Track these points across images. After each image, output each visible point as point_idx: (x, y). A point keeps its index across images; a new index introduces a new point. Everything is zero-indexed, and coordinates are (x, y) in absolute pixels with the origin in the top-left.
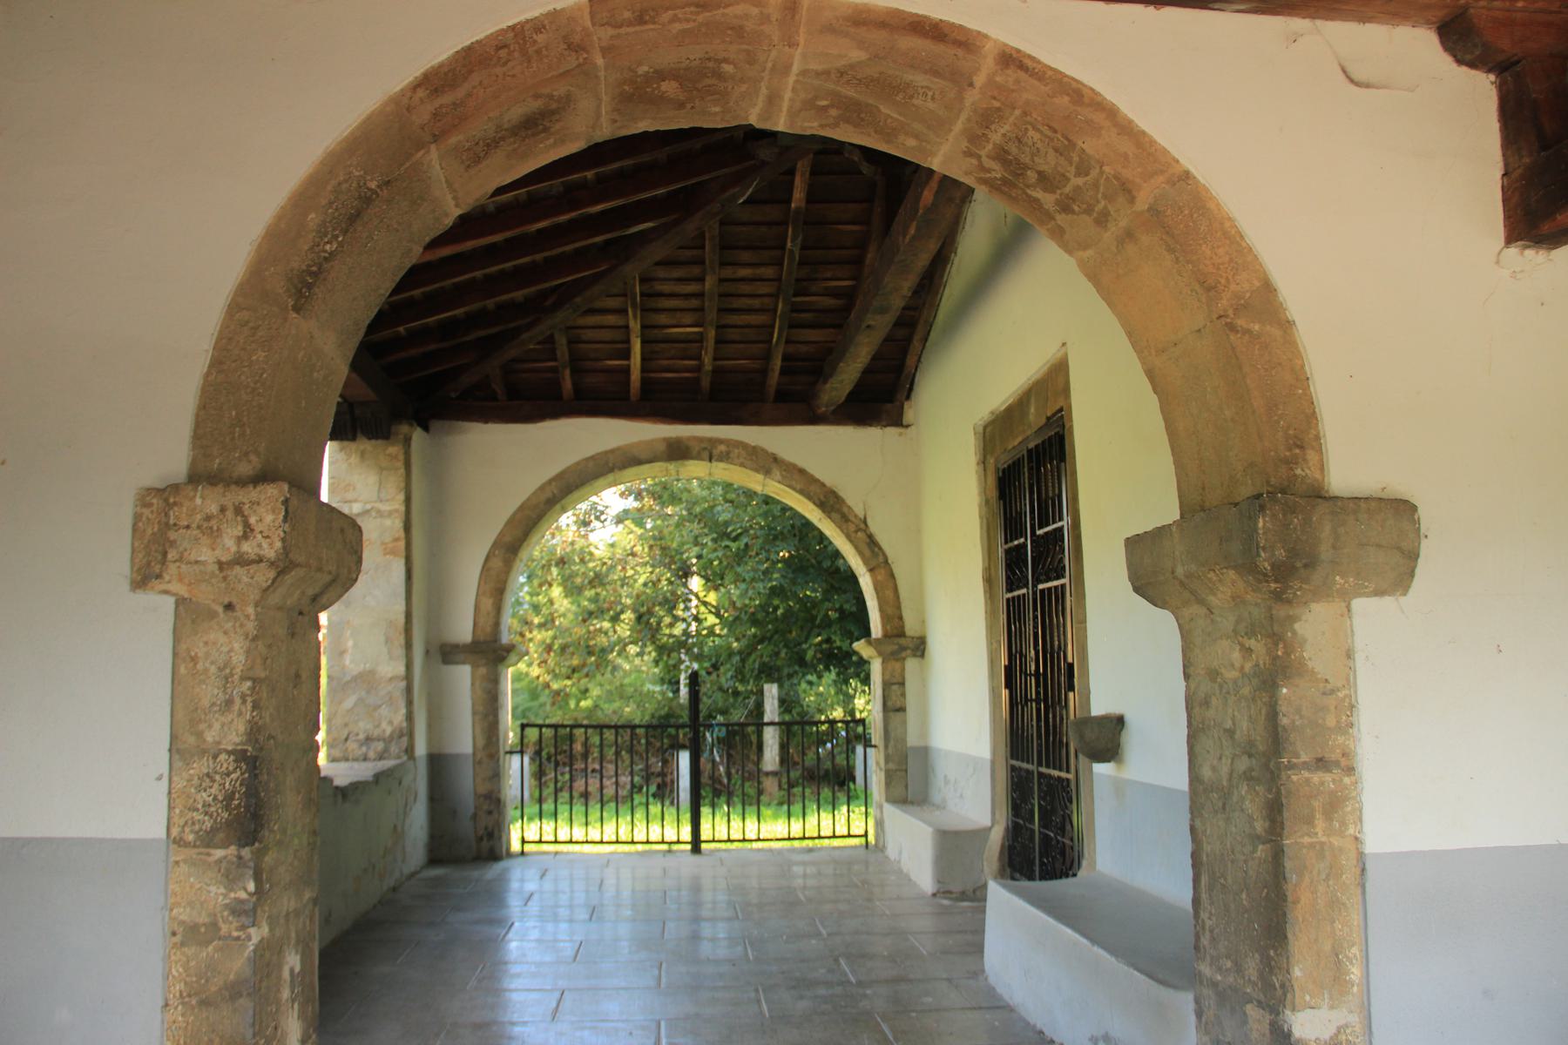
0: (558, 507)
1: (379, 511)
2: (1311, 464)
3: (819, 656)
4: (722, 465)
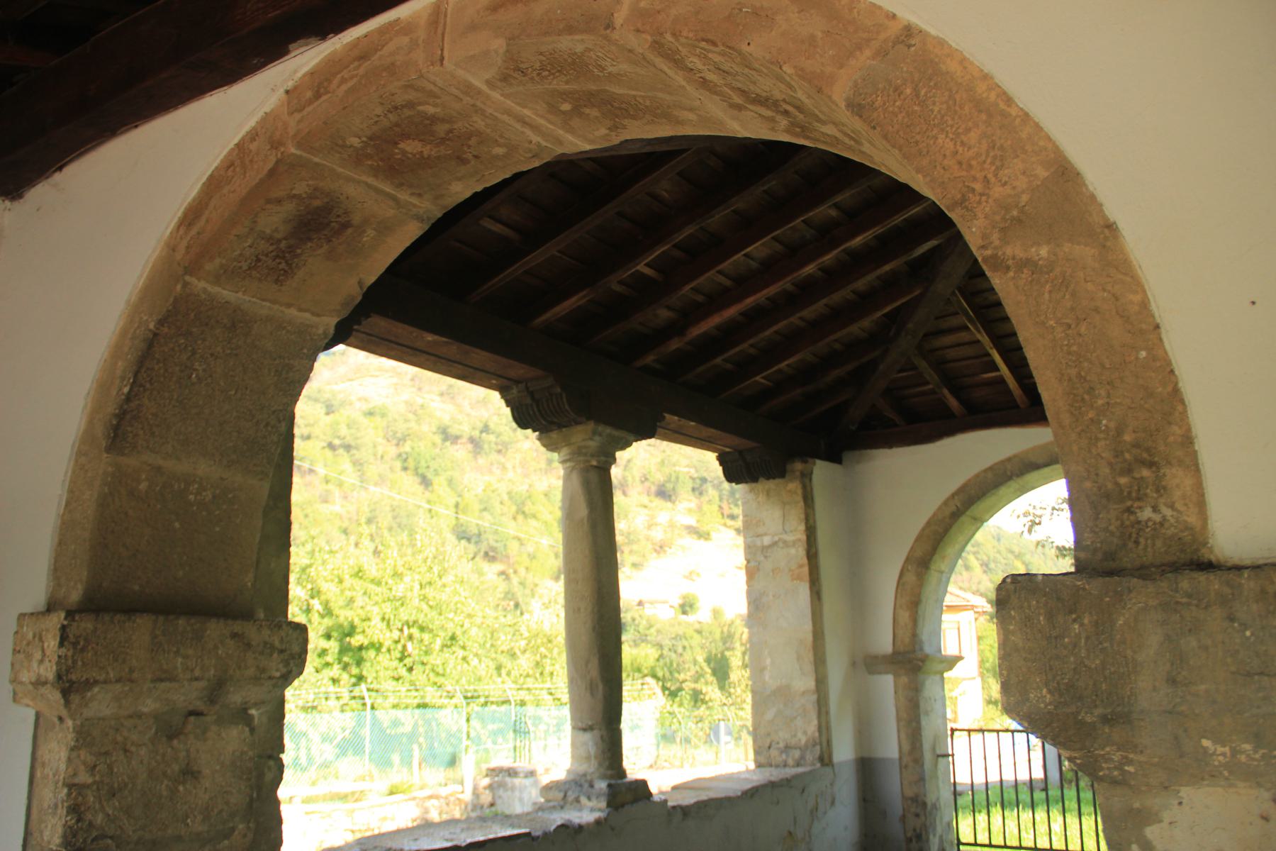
1: (785, 542)
2: (1177, 494)
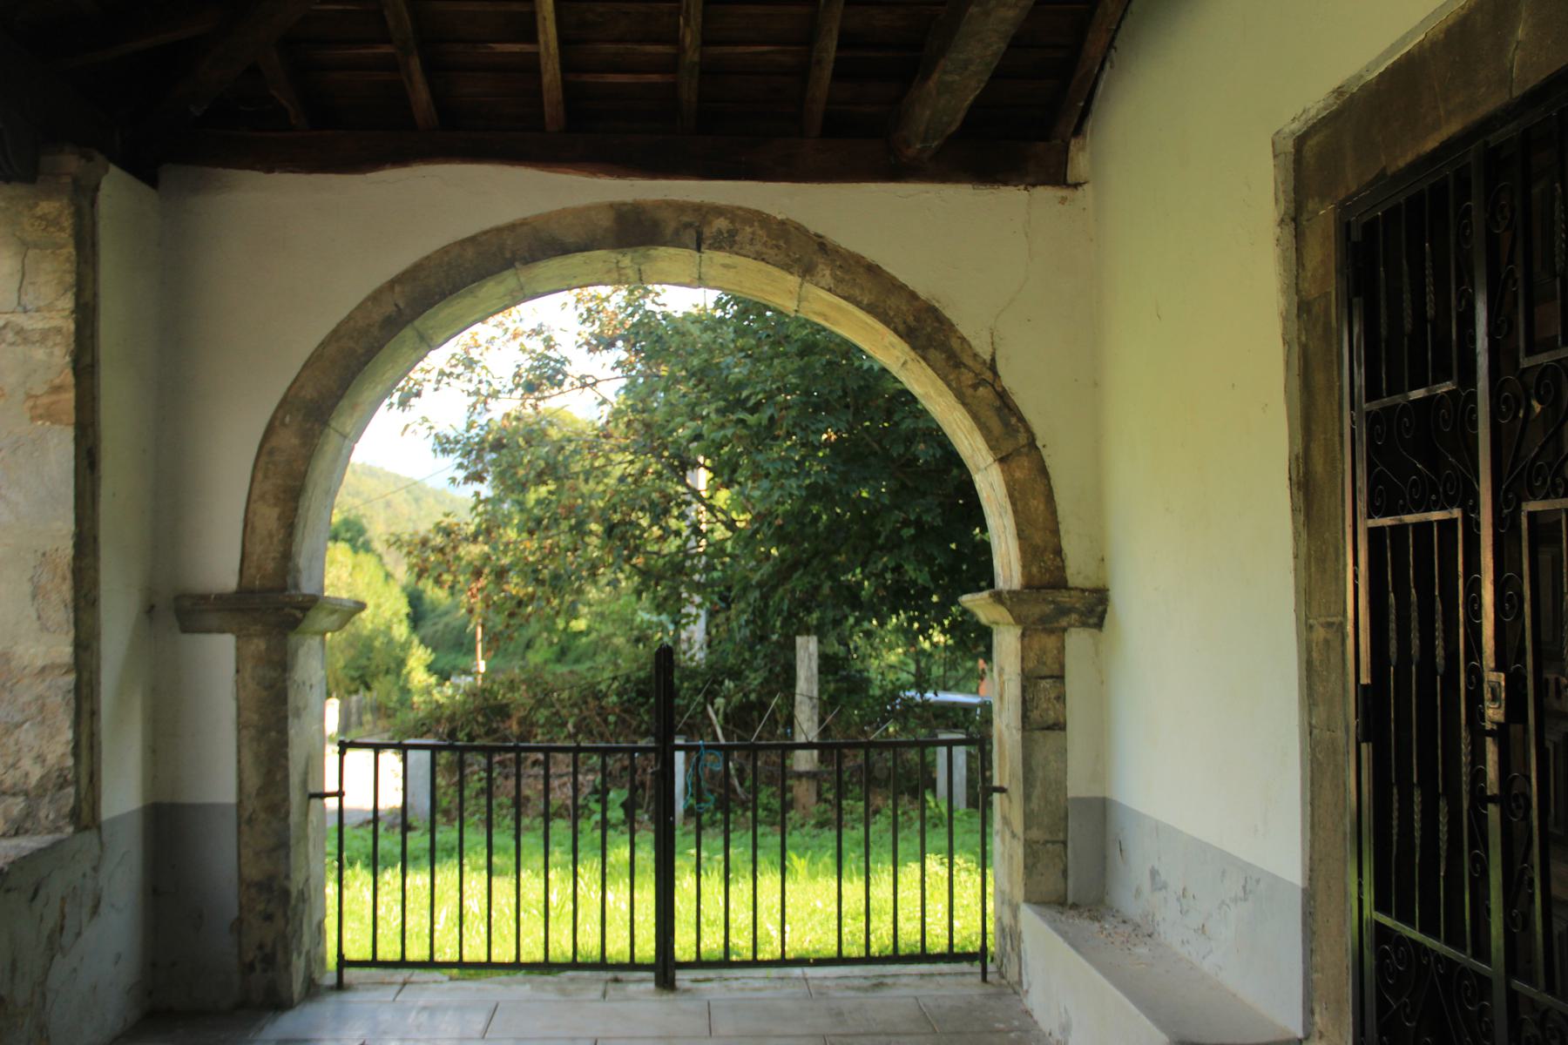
0: (408, 333)
1: (20, 331)
3: (882, 593)
4: (720, 257)
